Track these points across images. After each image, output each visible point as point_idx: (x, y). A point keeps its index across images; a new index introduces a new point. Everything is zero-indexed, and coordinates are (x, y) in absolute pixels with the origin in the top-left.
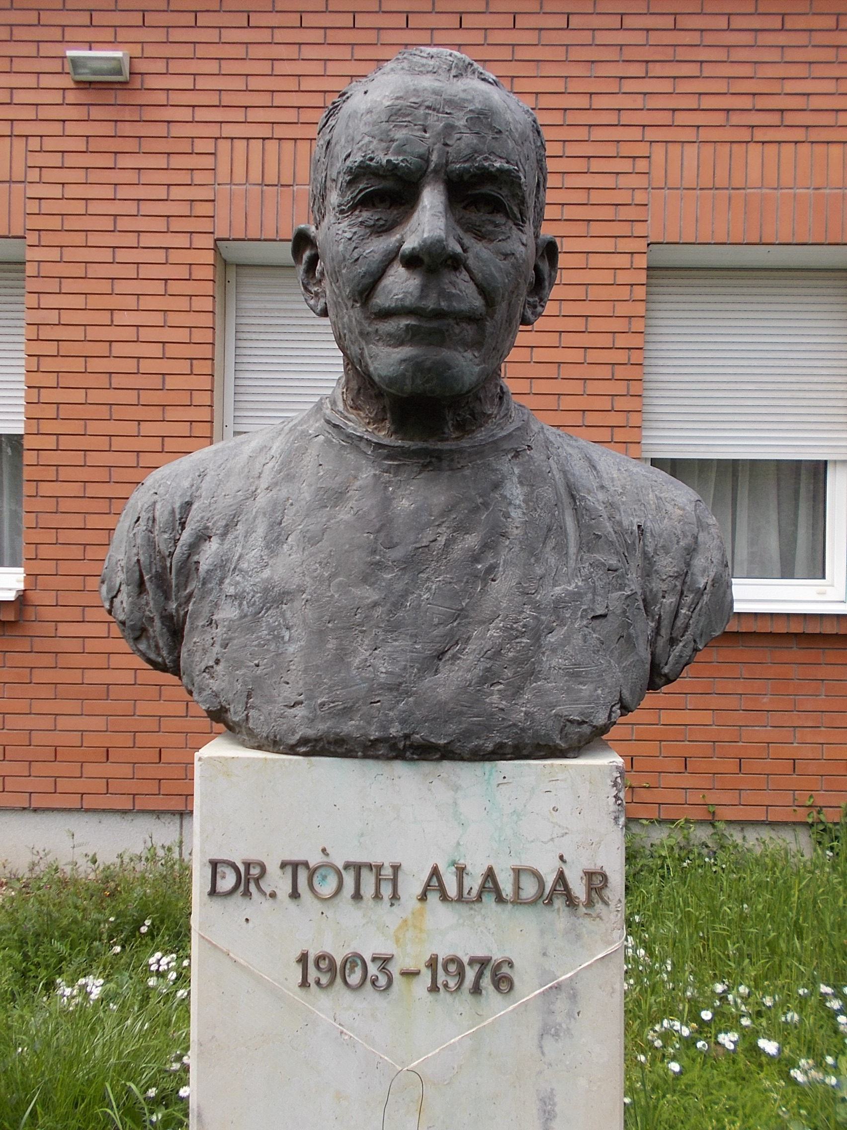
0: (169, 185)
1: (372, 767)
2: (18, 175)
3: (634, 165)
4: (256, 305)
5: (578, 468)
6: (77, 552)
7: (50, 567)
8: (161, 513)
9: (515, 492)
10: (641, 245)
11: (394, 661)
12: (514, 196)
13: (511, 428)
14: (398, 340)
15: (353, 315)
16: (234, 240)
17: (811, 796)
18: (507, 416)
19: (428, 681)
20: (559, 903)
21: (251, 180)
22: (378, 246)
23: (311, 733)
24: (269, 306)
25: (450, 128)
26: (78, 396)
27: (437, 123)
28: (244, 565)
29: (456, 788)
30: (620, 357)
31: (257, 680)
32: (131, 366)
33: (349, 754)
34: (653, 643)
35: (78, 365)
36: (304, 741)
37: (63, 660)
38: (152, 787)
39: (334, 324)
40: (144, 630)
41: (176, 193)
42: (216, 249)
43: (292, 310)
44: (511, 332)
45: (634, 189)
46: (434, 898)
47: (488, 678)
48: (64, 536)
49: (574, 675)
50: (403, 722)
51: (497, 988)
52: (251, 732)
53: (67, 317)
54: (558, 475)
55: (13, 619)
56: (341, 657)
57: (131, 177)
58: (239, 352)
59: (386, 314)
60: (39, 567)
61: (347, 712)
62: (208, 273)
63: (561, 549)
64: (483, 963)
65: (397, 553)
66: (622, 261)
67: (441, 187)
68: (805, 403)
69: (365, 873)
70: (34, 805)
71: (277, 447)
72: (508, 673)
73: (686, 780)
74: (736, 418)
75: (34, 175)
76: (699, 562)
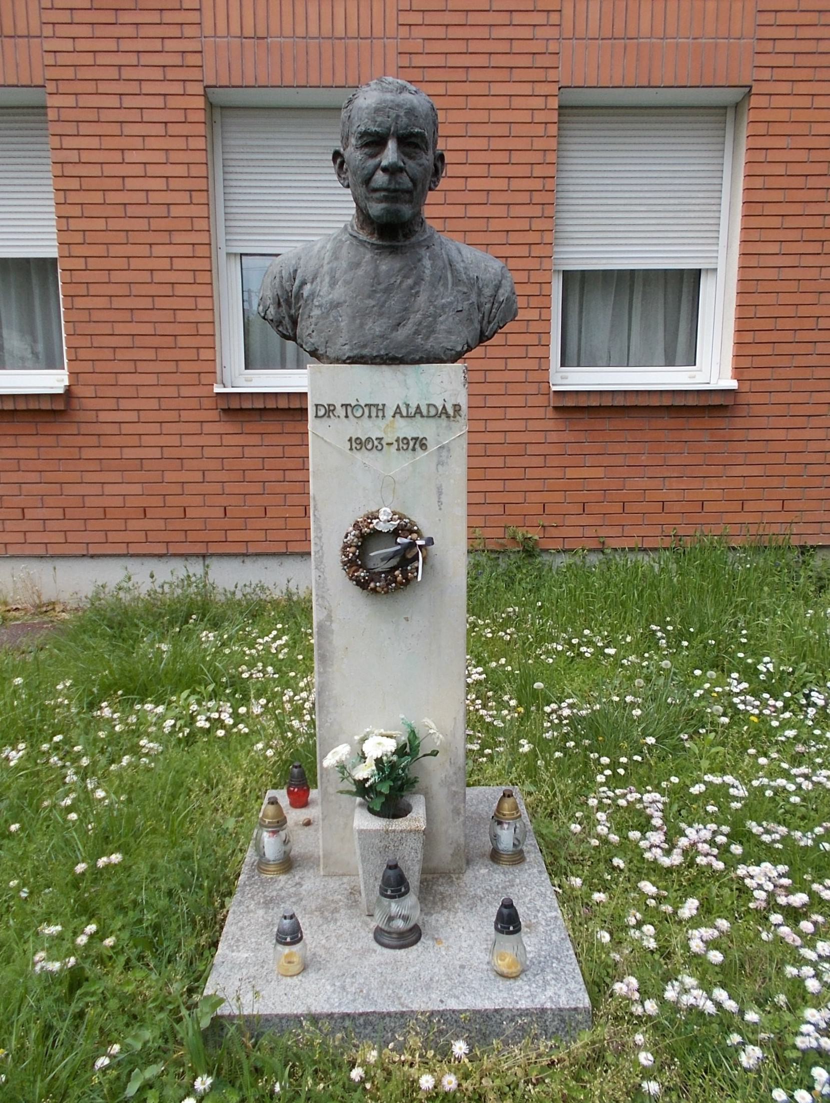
0: (163, 38)
1: (374, 368)
2: (35, 31)
3: (548, 18)
4: (241, 142)
5: (454, 254)
6: (108, 354)
7: (88, 367)
8: (285, 274)
9: (427, 263)
10: (553, 89)
11: (381, 327)
12: (423, 141)
13: (426, 236)
14: (380, 201)
15: (362, 190)
16: (220, 87)
17: (675, 529)
18: (424, 231)
19: (394, 334)
20: (443, 416)
21: (232, 33)
22: (372, 163)
23: (351, 354)
24: (250, 143)
25: (398, 116)
26: (100, 224)
27: (393, 114)
28: (321, 294)
29: (405, 375)
30: (537, 184)
31: (329, 337)
32: (140, 197)
33: (365, 363)
34: (481, 322)
35: (98, 197)
36: (349, 358)
37: (104, 441)
38: (180, 536)
39: (353, 194)
40: (281, 322)
41: (170, 45)
42: (205, 95)
43: (269, 146)
44: (423, 195)
45: (548, 40)
46: (398, 416)
47: (417, 333)
48: (98, 341)
49: (449, 332)
50: (386, 349)
51: (421, 447)
52: (328, 357)
53: (86, 156)
54: (445, 256)
55: (62, 408)
56: (362, 326)
57: (130, 31)
58: (227, 183)
59: (375, 190)
60: (80, 367)
61: (364, 346)
62: (200, 116)
63: (445, 285)
64: (416, 439)
65: (382, 287)
66: (538, 103)
67: (395, 140)
68: (684, 221)
69: (372, 408)
70: (91, 552)
71: (329, 246)
72: (424, 331)
73: (584, 520)
74: (631, 235)
75: (48, 31)
76: (501, 291)
